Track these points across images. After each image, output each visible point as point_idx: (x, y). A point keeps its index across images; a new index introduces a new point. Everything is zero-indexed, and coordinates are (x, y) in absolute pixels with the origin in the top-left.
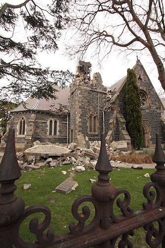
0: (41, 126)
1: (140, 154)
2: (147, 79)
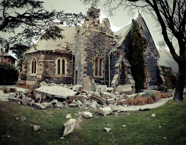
0: (50, 65)
1: (143, 96)
2: (146, 29)
